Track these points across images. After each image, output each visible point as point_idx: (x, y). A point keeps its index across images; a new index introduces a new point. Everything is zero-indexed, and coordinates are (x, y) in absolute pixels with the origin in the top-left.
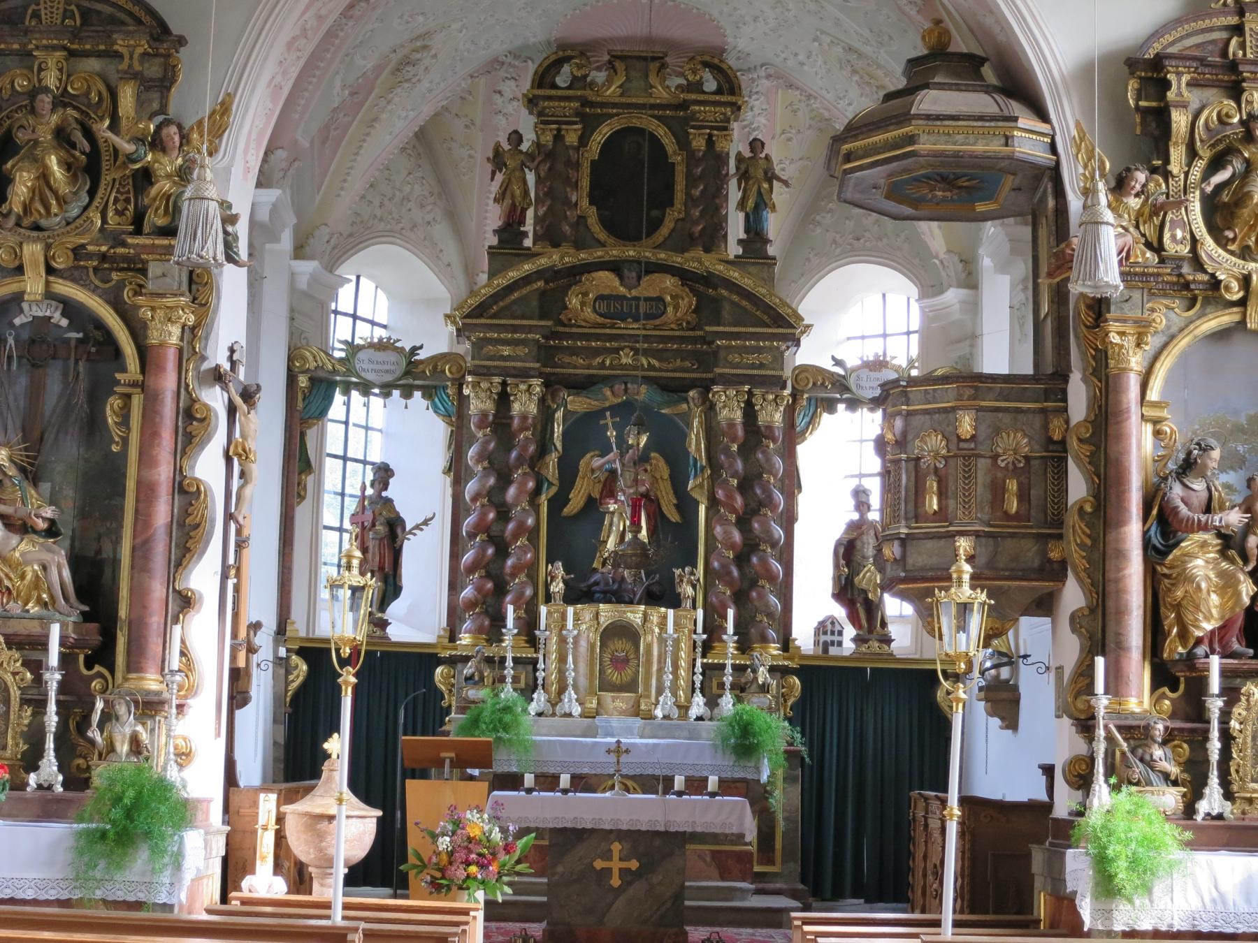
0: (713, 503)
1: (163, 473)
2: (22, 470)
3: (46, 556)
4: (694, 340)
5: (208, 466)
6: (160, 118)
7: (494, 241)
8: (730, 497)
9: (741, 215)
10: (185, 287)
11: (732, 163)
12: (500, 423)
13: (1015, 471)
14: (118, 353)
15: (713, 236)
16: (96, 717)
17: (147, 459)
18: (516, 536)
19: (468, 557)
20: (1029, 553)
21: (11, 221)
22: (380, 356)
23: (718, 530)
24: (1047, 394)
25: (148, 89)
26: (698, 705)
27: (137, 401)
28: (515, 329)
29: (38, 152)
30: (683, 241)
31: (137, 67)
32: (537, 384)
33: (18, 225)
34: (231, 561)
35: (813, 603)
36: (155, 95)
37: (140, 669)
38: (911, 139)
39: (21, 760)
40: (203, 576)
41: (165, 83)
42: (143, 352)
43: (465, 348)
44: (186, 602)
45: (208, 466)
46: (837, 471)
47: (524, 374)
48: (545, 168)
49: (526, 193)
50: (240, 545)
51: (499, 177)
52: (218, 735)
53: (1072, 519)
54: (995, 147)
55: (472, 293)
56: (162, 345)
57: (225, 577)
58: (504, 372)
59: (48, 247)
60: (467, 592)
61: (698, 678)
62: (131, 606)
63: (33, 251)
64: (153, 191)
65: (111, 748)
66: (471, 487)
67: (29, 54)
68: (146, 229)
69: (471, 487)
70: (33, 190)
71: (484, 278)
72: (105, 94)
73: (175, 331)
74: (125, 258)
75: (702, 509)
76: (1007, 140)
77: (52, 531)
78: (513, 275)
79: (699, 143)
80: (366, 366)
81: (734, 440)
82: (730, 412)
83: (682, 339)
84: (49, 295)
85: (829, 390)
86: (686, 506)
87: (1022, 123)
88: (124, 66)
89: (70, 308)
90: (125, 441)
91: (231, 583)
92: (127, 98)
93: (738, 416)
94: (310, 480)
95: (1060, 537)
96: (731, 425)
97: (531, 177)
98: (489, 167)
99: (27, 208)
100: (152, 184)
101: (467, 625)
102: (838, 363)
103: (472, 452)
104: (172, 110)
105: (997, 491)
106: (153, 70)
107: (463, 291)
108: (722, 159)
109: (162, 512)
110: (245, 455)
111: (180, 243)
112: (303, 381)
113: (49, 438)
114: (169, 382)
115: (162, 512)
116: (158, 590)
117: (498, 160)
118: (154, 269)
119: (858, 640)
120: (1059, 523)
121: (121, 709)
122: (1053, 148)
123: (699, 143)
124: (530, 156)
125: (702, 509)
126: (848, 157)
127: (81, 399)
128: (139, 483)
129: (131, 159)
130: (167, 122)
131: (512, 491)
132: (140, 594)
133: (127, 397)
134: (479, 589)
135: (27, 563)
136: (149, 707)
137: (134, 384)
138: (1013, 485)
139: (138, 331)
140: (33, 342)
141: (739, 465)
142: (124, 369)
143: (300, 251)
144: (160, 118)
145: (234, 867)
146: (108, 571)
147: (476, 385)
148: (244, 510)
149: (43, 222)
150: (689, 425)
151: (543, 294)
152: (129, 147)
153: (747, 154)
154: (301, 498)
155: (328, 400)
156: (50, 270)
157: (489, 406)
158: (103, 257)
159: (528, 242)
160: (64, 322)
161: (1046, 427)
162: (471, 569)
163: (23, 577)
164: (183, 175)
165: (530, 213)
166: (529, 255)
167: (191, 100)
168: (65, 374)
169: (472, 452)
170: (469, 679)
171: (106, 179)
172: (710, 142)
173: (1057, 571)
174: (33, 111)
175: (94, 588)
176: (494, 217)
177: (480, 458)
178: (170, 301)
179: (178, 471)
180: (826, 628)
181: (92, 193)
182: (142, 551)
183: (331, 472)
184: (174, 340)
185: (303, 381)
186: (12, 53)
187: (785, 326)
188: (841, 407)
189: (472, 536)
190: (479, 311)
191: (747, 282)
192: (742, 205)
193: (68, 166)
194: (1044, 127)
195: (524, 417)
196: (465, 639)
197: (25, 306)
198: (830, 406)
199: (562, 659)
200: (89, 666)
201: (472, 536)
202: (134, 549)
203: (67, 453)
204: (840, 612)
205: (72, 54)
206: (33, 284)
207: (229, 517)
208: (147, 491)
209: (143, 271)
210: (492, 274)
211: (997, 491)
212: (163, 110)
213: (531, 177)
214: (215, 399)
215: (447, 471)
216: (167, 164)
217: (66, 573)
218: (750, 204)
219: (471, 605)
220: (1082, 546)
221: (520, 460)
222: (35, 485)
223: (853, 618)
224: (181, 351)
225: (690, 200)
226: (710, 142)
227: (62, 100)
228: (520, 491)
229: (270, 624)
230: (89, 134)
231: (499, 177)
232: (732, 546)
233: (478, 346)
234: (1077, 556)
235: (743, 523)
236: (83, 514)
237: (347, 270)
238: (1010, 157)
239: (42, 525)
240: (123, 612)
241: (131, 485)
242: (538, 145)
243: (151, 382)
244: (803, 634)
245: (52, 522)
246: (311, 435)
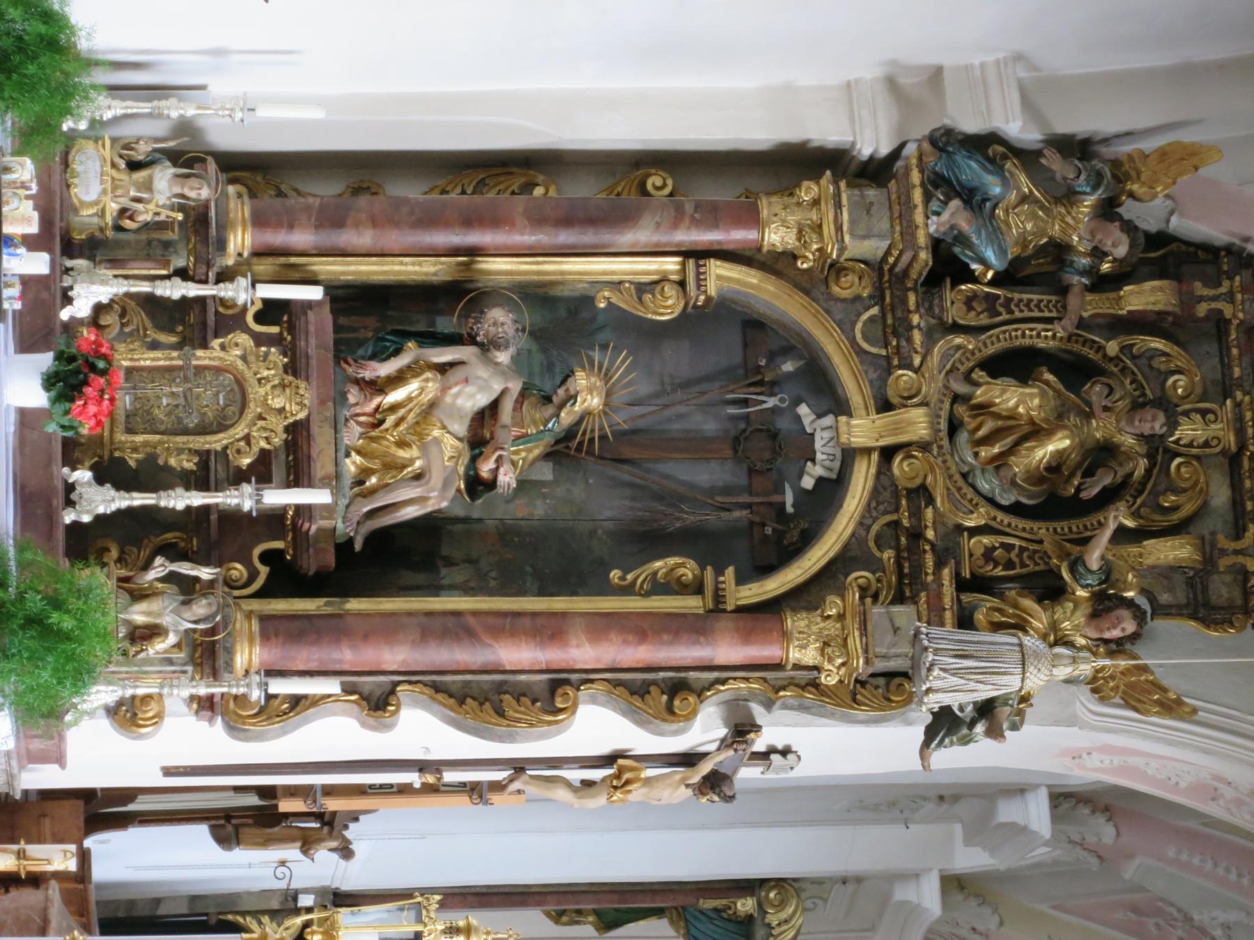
1: (582, 653)
2: (570, 434)
3: (436, 478)
5: (596, 726)
10: (880, 665)
14: (766, 570)
16: (185, 569)
17: (602, 625)
21: (961, 388)
25: (1190, 583)
27: (692, 603)
29: (1073, 419)
31: (1224, 563)
33: (956, 398)
34: (450, 777)
36: (1181, 596)
37: (265, 637)
40: (421, 730)
41: (1204, 611)
42: (772, 608)
44: (377, 704)
45: (596, 726)
50: (475, 791)
52: (168, 772)
56: (785, 636)
57: (421, 766)
59: (924, 446)
62: (360, 615)
63: (917, 423)
64: (1028, 603)
65: (138, 596)
67: (1226, 393)
68: (966, 598)
70: (1012, 416)
72: (1175, 517)
73: (810, 656)
74: (918, 568)
77: (477, 486)
84: (849, 455)
88: (1223, 542)
89: (831, 491)
90: (627, 590)
91: (413, 778)
92: (1172, 551)
94: (1234, 249)
99: (983, 409)
104: (1161, 625)
106: (1222, 589)
109: (519, 655)
110: (619, 783)
112: (746, 905)
113: (624, 474)
114: (728, 651)
115: (519, 655)
116: (395, 656)
121: (201, 608)
127: (690, 518)
128: (564, 615)
129: (1076, 564)
132: (388, 628)
133: (697, 588)
135: (424, 448)
136: (206, 653)
137: (719, 598)
139: (804, 596)
140: (774, 435)
142: (741, 580)
143: (954, 884)
146: (420, 578)
148: (532, 790)
149: (963, 437)
152: (1094, 559)
156: (888, 453)
158: (916, 535)
160: (808, 483)
163: (402, 444)
167: (1177, 651)
168: (727, 490)
171: (1042, 529)
174: (1137, 406)
175: (394, 557)
178: (855, 641)
179: (586, 677)
181: (1016, 509)
182: (456, 628)
184: (795, 655)
185: (746, 905)
186: (1226, 367)
193: (1055, 467)
197: (828, 420)
200: (266, 557)
202: (457, 614)
203: (602, 502)
205: (1233, 460)
206: (863, 429)
207: (519, 767)
208: (550, 629)
209: (899, 599)
212: (1160, 610)
214: (704, 729)
217: (411, 512)
222: (548, 456)
224: (778, 666)
227: (1158, 450)
229: (351, 876)
230: (1108, 497)
236: (508, 534)
239: (485, 469)
240: (354, 604)
241: (559, 603)
243: (725, 623)
245: (491, 484)
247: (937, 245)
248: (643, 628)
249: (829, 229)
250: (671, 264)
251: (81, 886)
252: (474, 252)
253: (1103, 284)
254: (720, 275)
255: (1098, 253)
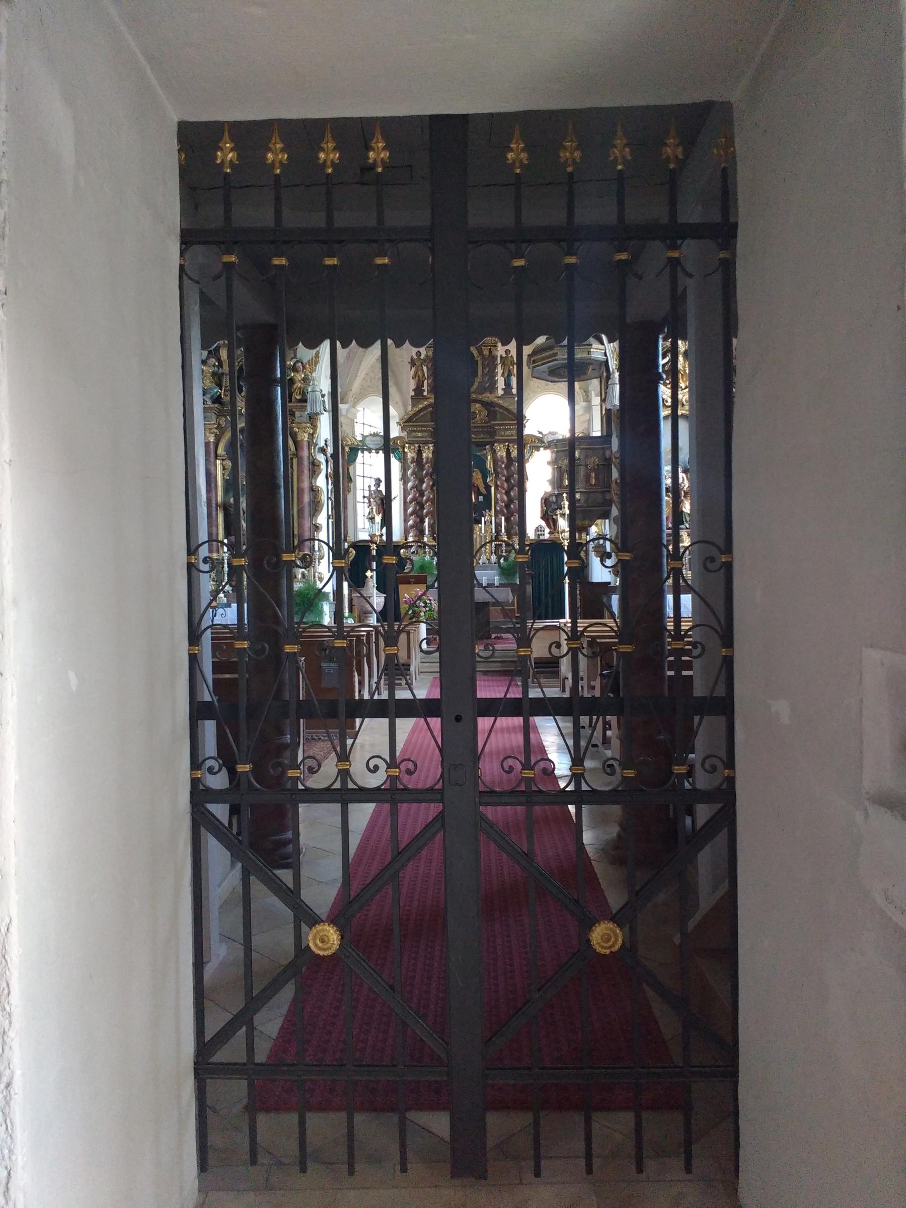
0: (497, 486)
1: (306, 485)
4: (487, 427)
6: (295, 360)
7: (413, 394)
8: (502, 484)
9: (503, 379)
11: (499, 359)
12: (419, 461)
13: (593, 470)
15: (493, 387)
18: (427, 502)
19: (410, 510)
20: (599, 498)
22: (374, 439)
23: (499, 496)
24: (604, 443)
26: (494, 558)
27: (295, 461)
28: (422, 426)
30: (482, 390)
32: (431, 446)
35: (534, 520)
38: (556, 354)
39: (292, 564)
43: (404, 434)
44: (317, 528)
46: (540, 475)
47: (426, 443)
48: (430, 365)
49: (424, 374)
51: (413, 369)
53: (613, 485)
54: (585, 355)
55: (406, 414)
56: (302, 440)
58: (418, 442)
60: (411, 522)
61: (493, 549)
66: (410, 485)
68: (293, 400)
69: (410, 485)
71: (410, 408)
73: (306, 435)
75: (493, 489)
76: (589, 352)
78: (421, 406)
79: (486, 352)
80: (369, 443)
81: (503, 463)
82: (502, 453)
83: (483, 427)
85: (539, 443)
86: (488, 488)
87: (594, 346)
93: (504, 454)
94: (352, 485)
95: (609, 491)
96: (502, 457)
97: (425, 368)
98: (409, 365)
100: (294, 384)
101: (411, 534)
102: (540, 433)
103: (409, 472)
104: (298, 357)
105: (588, 477)
107: (403, 413)
108: (495, 358)
109: (306, 498)
111: (308, 405)
112: (347, 449)
114: (305, 453)
115: (306, 498)
116: (307, 524)
117: (413, 363)
118: (297, 414)
119: (550, 533)
120: (610, 486)
122: (605, 354)
123: (486, 352)
124: (424, 360)
125: (493, 489)
126: (534, 362)
128: (298, 489)
130: (298, 361)
131: (424, 485)
132: (300, 526)
134: (415, 522)
137: (293, 454)
138: (593, 475)
141: (505, 472)
144: (295, 360)
145: (338, 615)
147: (409, 448)
150: (487, 458)
151: (432, 412)
153: (504, 355)
154: (349, 491)
155: (356, 455)
157: (414, 455)
159: (425, 394)
161: (604, 453)
162: (411, 515)
164: (306, 380)
165: (426, 382)
166: (426, 398)
169: (409, 472)
170: (413, 553)
172: (490, 351)
173: (609, 503)
176: (413, 384)
177: (413, 473)
178: (304, 425)
180: (538, 529)
182: (300, 511)
183: (359, 482)
184: (306, 439)
185: (347, 449)
187: (520, 419)
188: (542, 449)
189: (411, 502)
190: (409, 420)
191: (505, 405)
192: (503, 375)
194: (602, 347)
195: (427, 458)
196: (411, 539)
198: (538, 449)
199: (658, 1068)
201: (411, 502)
204: (543, 523)
208: (300, 491)
210: (413, 406)
211: (588, 477)
212: (295, 357)
213: (425, 368)
214: (321, 458)
215: (401, 480)
216: (300, 376)
218: (506, 375)
219: (412, 527)
220: (616, 494)
221: (427, 474)
223: (549, 526)
225: (483, 375)
226: (490, 351)
228: (427, 486)
231: (413, 369)
232: (504, 501)
233: (409, 433)
234: (615, 498)
235: (507, 493)
237: (360, 408)
238: (590, 359)
240: (296, 532)
242: (427, 356)
243: (300, 454)
244: (531, 533)
246: (351, 468)
247: (213, 403)
248: (300, 472)
249: (210, 427)
250: (218, 462)
251: (226, 128)
252: (217, 505)
253: (221, 365)
254: (221, 451)
255: (214, 365)
